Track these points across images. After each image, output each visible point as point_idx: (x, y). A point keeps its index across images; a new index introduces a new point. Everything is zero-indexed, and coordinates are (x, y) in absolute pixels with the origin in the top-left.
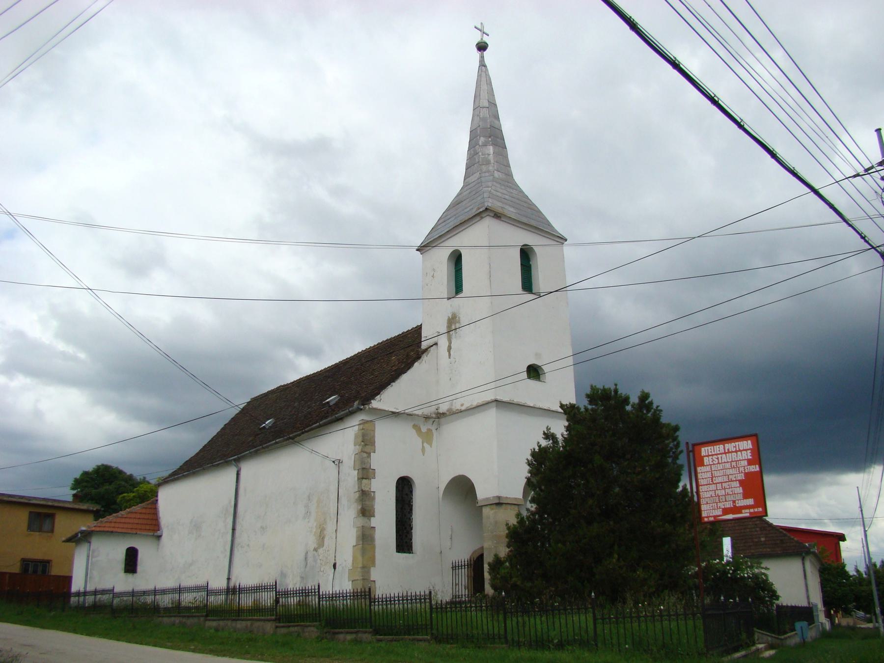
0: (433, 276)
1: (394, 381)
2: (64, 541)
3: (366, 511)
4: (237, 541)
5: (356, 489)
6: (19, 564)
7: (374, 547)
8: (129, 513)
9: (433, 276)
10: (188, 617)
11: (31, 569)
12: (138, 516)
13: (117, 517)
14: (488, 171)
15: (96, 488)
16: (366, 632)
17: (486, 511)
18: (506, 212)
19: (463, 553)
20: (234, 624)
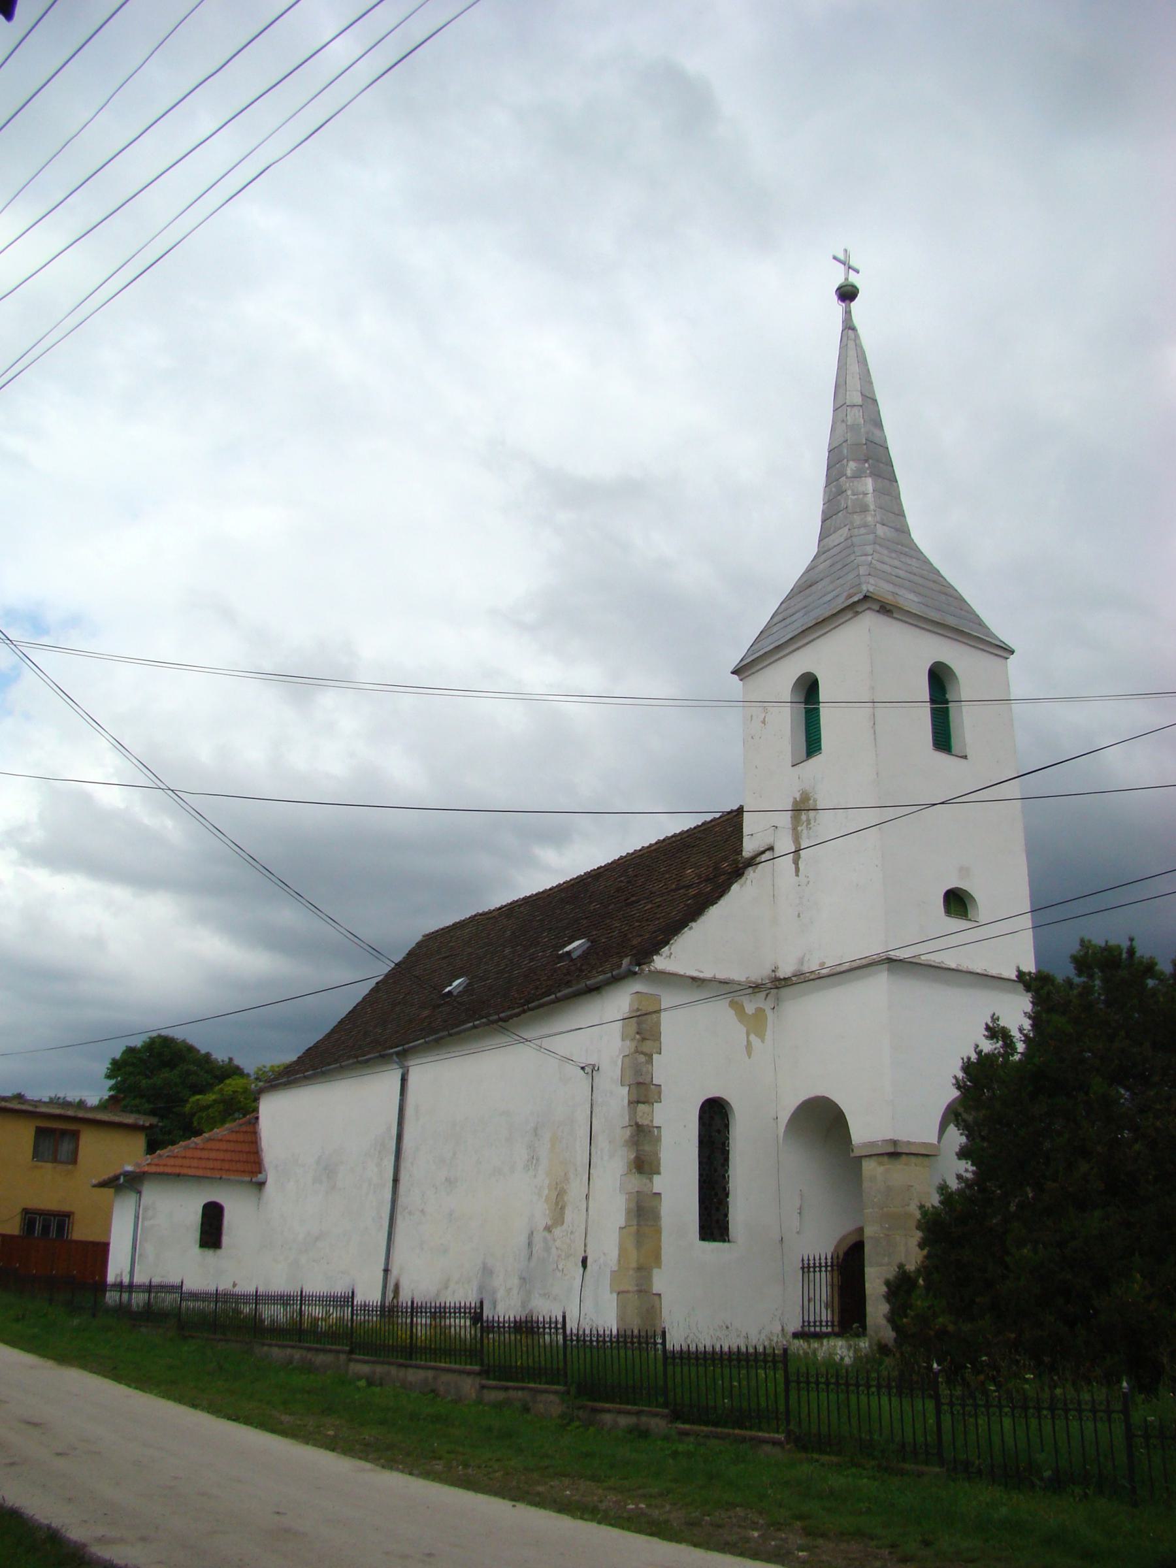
0: (764, 722)
1: (694, 919)
2: (95, 1186)
3: (644, 1164)
4: (402, 1200)
5: (626, 1121)
6: (18, 1219)
7: (658, 1231)
8: (210, 1139)
9: (764, 722)
10: (317, 1350)
11: (38, 1227)
12: (224, 1146)
13: (186, 1148)
14: (865, 526)
15: (147, 1077)
16: (656, 1415)
17: (869, 1167)
18: (902, 603)
19: (821, 1242)
20: (402, 1373)
